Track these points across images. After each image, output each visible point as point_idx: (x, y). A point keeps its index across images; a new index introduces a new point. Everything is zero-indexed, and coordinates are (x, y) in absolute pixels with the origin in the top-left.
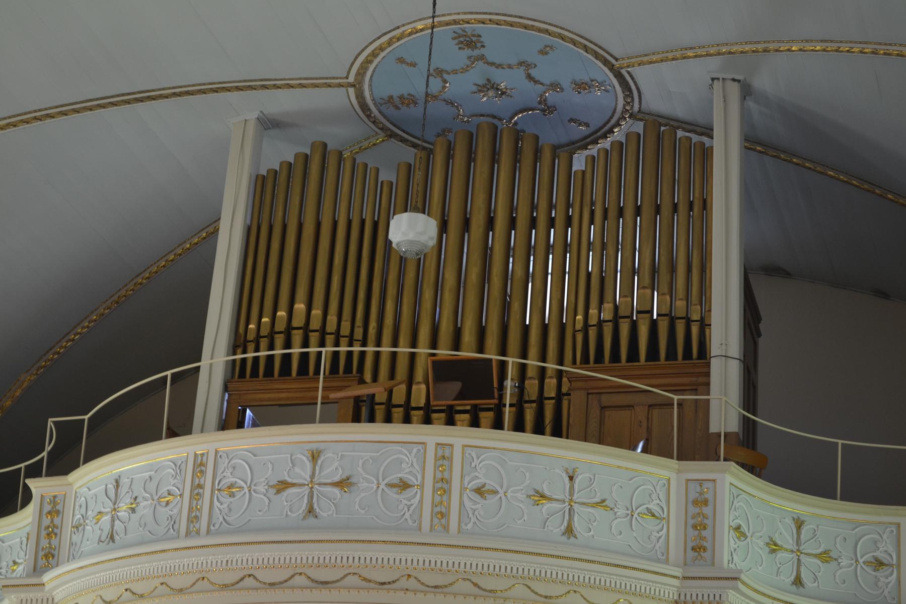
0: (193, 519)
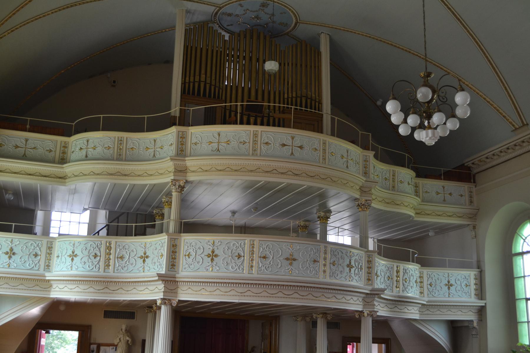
0: (255, 150)
